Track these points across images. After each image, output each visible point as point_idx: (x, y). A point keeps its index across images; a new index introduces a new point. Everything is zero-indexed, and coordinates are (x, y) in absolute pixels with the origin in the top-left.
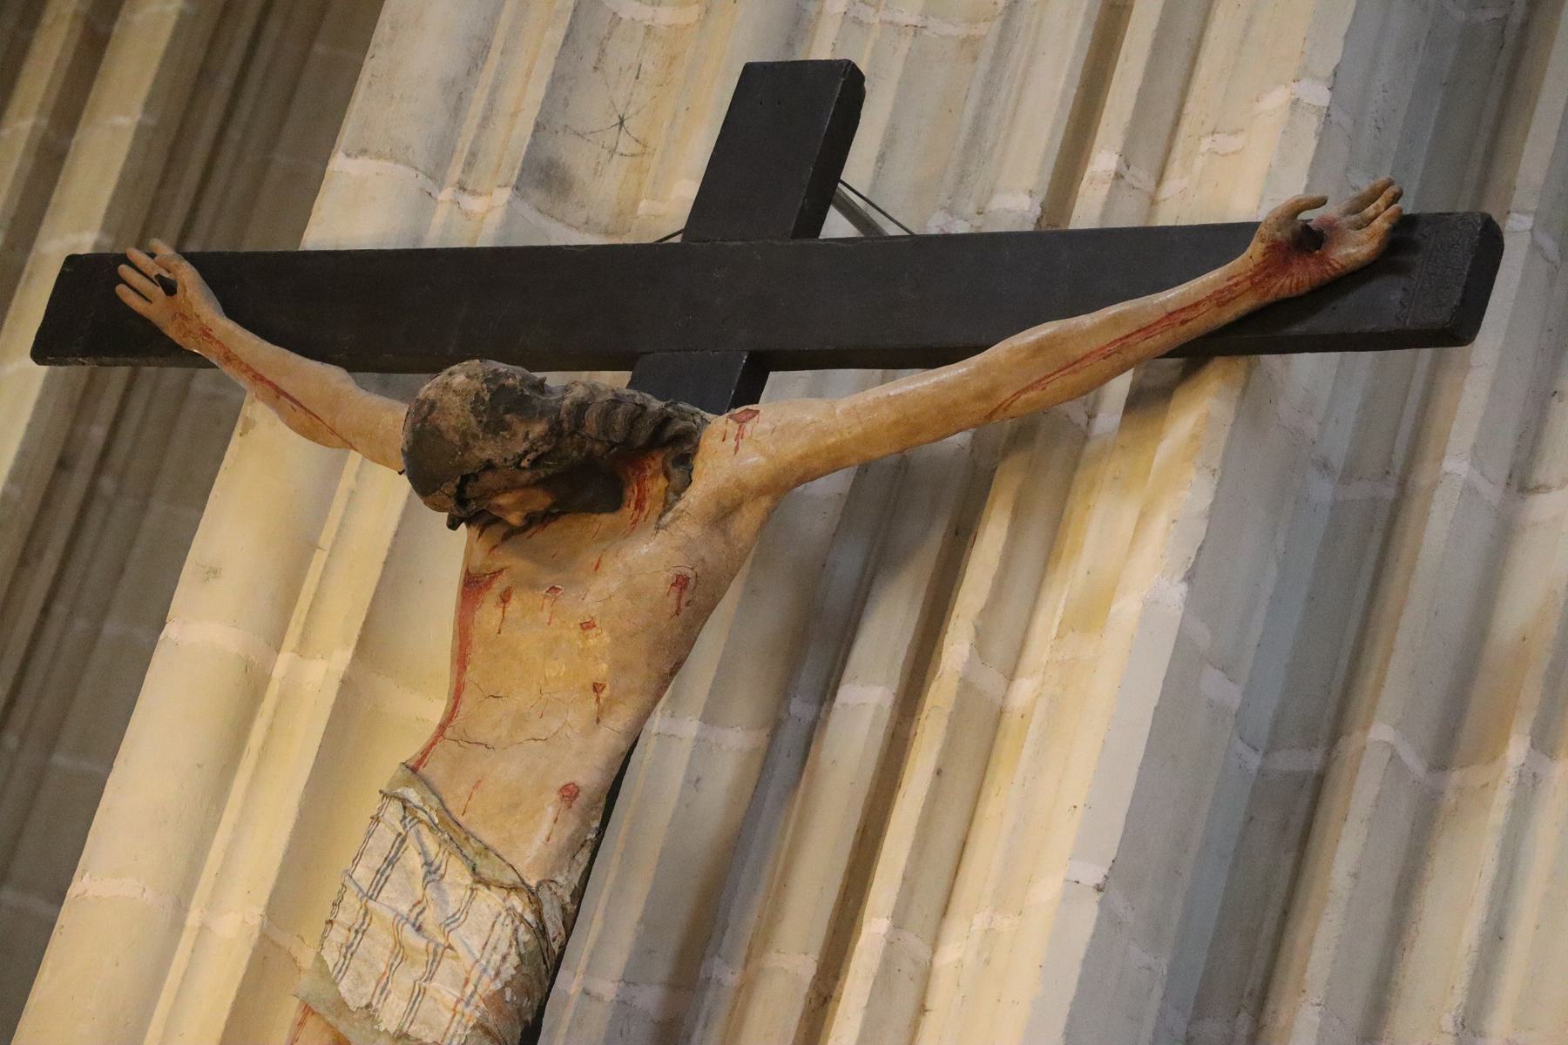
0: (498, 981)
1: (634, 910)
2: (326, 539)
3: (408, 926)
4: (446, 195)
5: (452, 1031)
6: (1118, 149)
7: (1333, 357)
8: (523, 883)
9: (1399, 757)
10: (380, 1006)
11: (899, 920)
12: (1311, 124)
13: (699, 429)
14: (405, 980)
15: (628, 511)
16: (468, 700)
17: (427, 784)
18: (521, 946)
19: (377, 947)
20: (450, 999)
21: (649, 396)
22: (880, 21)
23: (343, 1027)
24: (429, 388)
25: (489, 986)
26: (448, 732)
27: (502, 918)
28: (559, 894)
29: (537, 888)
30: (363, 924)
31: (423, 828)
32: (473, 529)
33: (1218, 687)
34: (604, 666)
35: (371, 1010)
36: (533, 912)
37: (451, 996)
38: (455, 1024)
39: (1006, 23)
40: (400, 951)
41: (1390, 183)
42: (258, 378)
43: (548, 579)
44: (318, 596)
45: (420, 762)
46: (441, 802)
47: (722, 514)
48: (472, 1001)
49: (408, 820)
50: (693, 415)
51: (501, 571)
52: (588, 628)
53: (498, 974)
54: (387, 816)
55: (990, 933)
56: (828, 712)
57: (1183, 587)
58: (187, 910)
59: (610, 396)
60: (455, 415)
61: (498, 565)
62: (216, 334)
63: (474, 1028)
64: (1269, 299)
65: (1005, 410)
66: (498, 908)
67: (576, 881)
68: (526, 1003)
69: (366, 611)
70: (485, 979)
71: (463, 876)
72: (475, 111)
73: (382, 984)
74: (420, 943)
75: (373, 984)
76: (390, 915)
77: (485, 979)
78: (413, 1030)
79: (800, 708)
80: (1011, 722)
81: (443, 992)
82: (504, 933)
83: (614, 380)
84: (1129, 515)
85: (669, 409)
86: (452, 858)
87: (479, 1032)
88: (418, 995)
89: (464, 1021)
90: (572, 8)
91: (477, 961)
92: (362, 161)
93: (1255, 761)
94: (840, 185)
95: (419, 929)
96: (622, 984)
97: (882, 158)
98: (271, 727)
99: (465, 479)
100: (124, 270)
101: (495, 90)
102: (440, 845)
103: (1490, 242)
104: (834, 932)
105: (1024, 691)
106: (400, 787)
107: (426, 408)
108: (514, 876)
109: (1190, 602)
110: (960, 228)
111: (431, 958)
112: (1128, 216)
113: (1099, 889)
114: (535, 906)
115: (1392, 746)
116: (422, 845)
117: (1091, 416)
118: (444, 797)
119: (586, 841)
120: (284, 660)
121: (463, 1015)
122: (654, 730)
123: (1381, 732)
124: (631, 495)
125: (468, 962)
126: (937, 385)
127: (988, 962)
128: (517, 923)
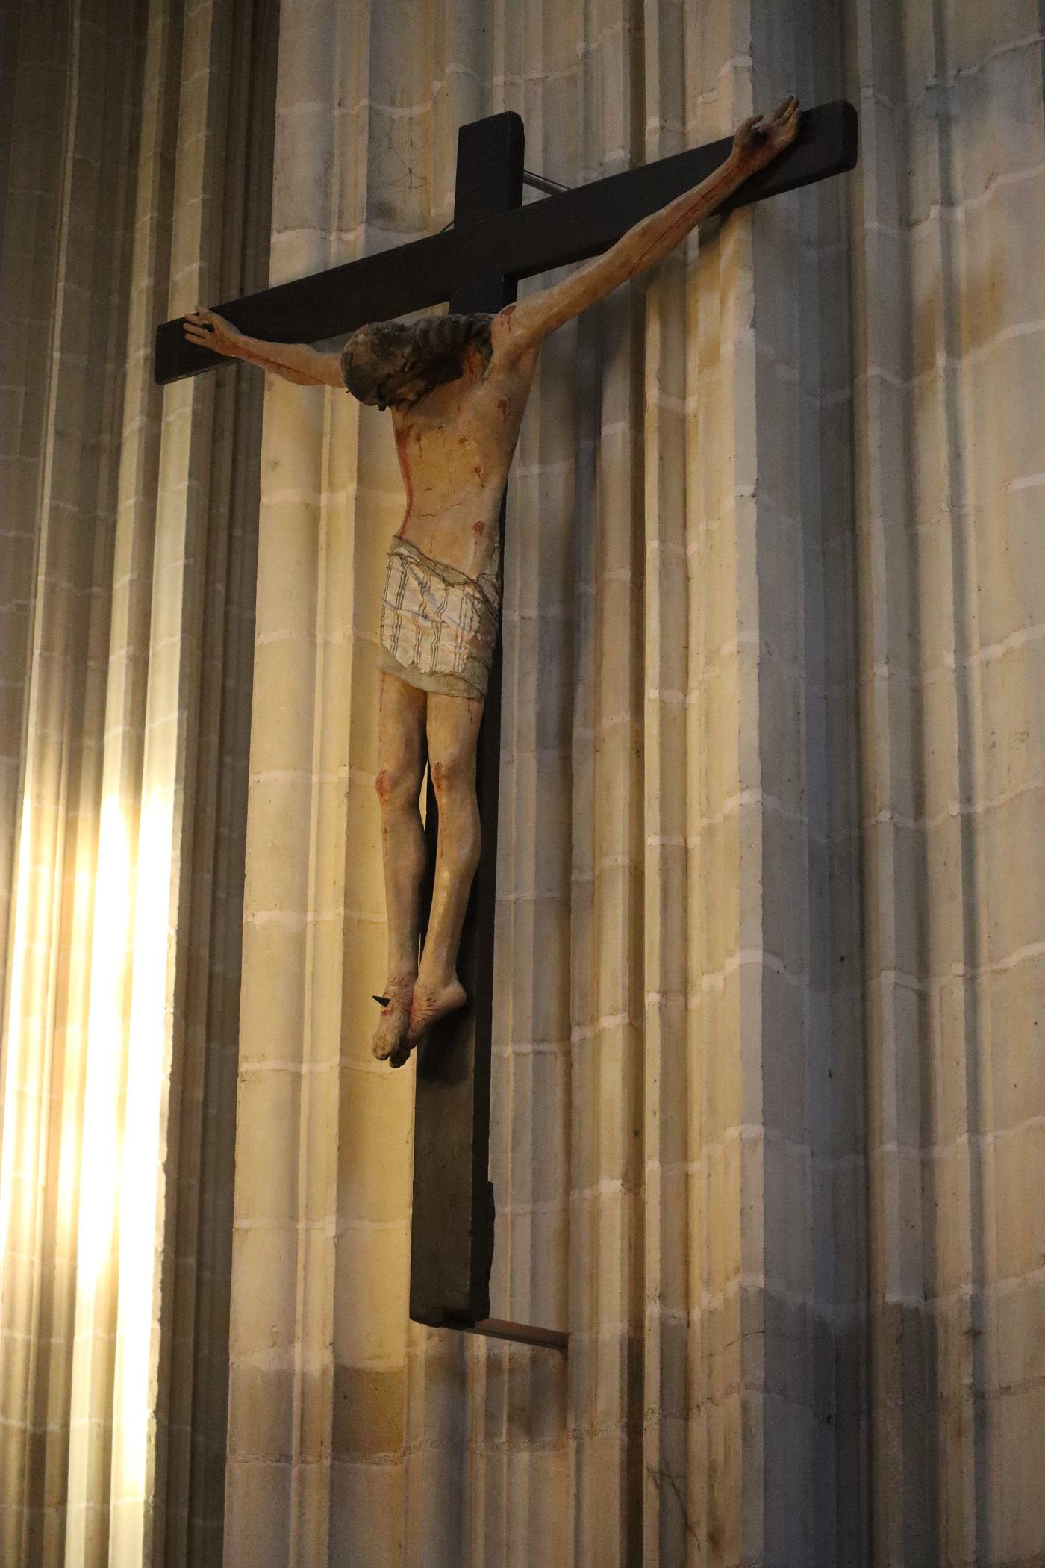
1: (534, 569)
2: (327, 428)
3: (420, 617)
4: (333, 236)
5: (457, 664)
7: (794, 193)
8: (470, 579)
9: (886, 380)
11: (663, 540)
12: (746, 77)
13: (489, 324)
14: (426, 645)
15: (467, 375)
16: (416, 494)
17: (409, 543)
18: (478, 611)
19: (409, 632)
20: (452, 648)
21: (458, 315)
23: (403, 677)
24: (348, 346)
25: (468, 636)
26: (411, 515)
27: (464, 600)
31: (413, 566)
34: (478, 458)
35: (415, 664)
36: (479, 592)
38: (457, 660)
39: (585, 64)
41: (792, 98)
42: (267, 361)
43: (437, 423)
44: (331, 460)
46: (418, 549)
47: (513, 363)
51: (412, 426)
52: (463, 441)
53: (470, 629)
54: (394, 565)
56: (600, 441)
57: (752, 331)
58: (315, 636)
60: (365, 358)
61: (409, 423)
62: (241, 345)
63: (467, 659)
64: (750, 173)
66: (461, 596)
67: (496, 570)
68: (489, 638)
70: (465, 633)
71: (440, 585)
72: (335, 189)
73: (416, 650)
74: (428, 624)
75: (412, 650)
76: (410, 615)
78: (438, 668)
79: (586, 444)
80: (690, 420)
82: (467, 607)
83: (439, 310)
85: (471, 319)
86: (432, 577)
87: (471, 659)
88: (435, 651)
90: (368, 122)
91: (459, 625)
93: (818, 403)
95: (426, 617)
99: (380, 386)
100: (186, 326)
101: (342, 175)
103: (849, 116)
105: (692, 403)
106: (395, 548)
107: (349, 357)
113: (754, 496)
116: (415, 574)
117: (685, 253)
122: (518, 476)
123: (873, 371)
124: (466, 366)
125: (454, 627)
126: (600, 266)
127: (711, 547)
128: (472, 600)
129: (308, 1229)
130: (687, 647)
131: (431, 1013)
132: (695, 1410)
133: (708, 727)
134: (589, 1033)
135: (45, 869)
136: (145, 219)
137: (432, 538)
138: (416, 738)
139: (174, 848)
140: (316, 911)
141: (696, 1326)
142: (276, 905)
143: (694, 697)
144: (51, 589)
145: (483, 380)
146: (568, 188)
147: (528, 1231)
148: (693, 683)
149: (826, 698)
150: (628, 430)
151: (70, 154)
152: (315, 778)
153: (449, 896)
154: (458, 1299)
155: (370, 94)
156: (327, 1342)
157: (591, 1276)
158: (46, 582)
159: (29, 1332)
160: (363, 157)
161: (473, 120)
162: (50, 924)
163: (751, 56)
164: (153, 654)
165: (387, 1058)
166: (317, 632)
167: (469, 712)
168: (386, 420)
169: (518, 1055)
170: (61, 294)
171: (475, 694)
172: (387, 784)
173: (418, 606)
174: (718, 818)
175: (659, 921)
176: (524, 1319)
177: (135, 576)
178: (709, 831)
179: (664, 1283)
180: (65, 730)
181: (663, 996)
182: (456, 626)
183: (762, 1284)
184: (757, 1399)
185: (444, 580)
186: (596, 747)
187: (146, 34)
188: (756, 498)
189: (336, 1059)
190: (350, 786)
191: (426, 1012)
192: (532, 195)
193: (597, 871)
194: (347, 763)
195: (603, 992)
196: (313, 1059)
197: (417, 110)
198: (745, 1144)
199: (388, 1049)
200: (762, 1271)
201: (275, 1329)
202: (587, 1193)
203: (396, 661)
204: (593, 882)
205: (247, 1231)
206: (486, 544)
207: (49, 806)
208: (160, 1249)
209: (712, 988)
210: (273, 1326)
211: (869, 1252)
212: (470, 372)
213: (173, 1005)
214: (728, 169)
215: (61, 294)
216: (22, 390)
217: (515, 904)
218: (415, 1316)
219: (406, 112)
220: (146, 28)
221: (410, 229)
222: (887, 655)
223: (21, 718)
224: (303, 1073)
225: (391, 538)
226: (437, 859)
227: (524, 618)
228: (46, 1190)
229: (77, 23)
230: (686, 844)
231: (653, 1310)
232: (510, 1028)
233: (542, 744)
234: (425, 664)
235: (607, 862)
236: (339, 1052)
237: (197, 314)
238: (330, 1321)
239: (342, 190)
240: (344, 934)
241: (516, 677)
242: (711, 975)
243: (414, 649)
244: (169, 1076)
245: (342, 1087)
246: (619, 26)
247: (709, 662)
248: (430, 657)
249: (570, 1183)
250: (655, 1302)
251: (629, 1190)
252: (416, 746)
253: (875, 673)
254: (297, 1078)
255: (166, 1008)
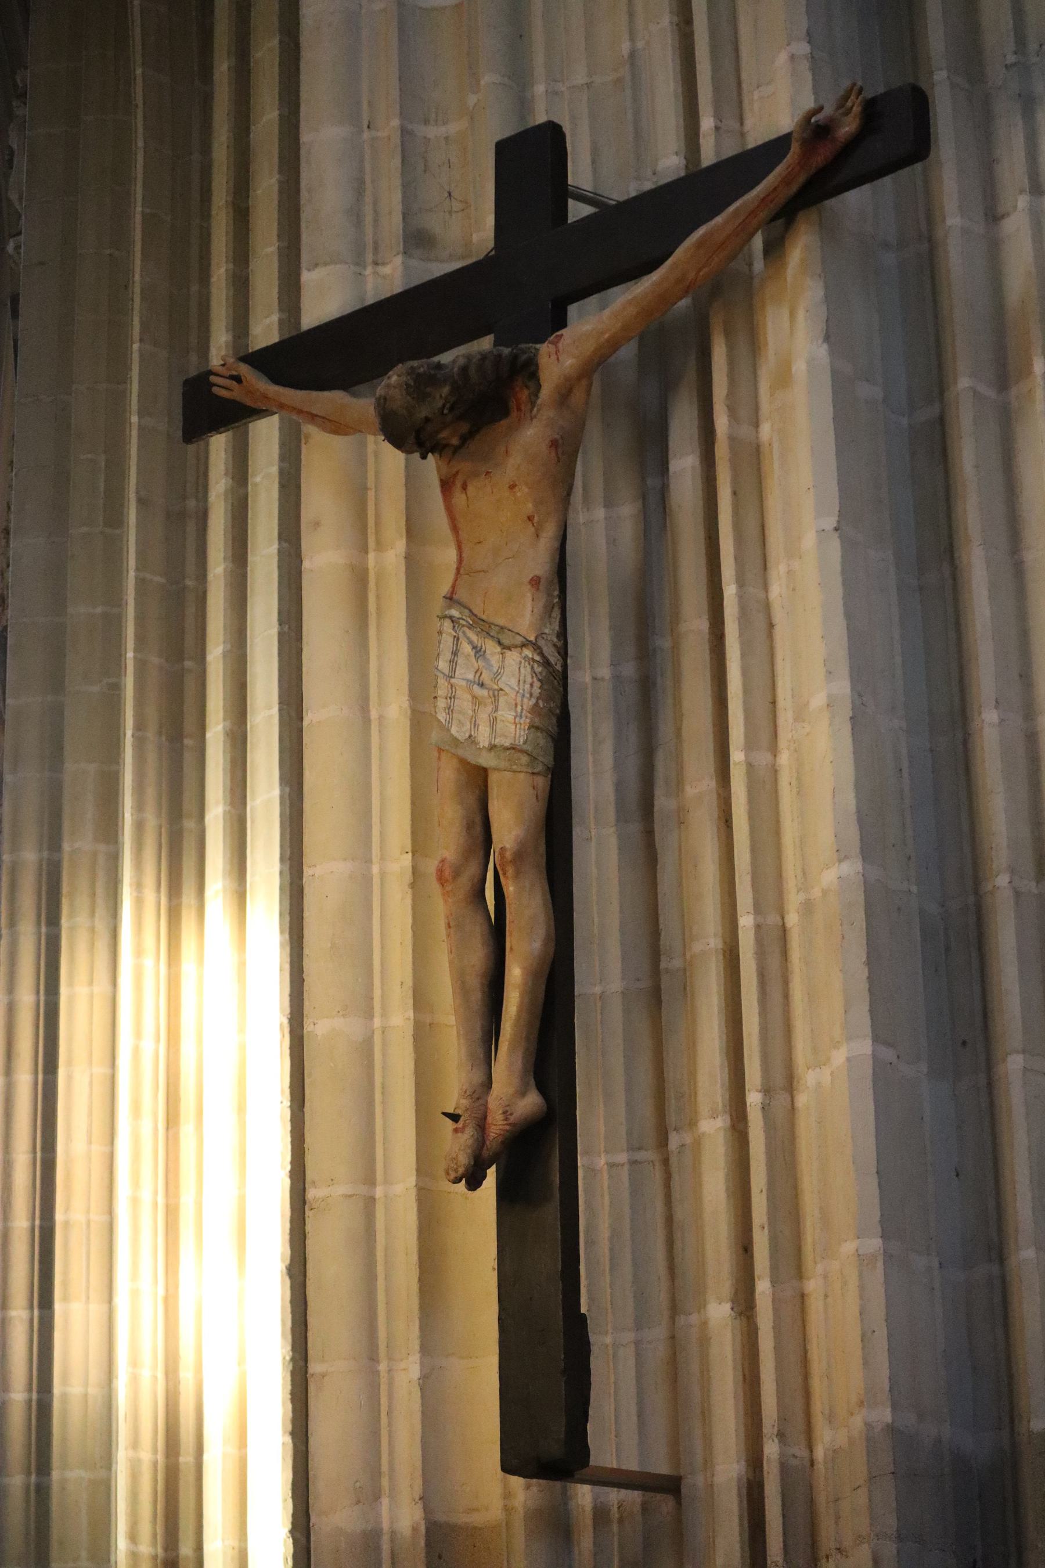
0: (532, 699)
2: (371, 482)
3: (475, 686)
4: (369, 271)
5: (518, 733)
6: (712, 113)
7: (866, 188)
8: (527, 640)
10: (476, 734)
11: (741, 582)
12: (804, 67)
14: (483, 716)
15: (514, 414)
17: (460, 604)
18: (539, 675)
19: (464, 702)
20: (511, 718)
22: (567, 88)
23: (460, 752)
24: (380, 390)
26: (462, 571)
27: (523, 664)
28: (549, 639)
29: (536, 640)
30: (452, 693)
31: (466, 629)
32: (436, 455)
33: (867, 391)
34: (530, 505)
36: (538, 654)
37: (510, 716)
38: (518, 731)
39: (632, 64)
40: (475, 699)
41: (854, 84)
45: (452, 593)
47: (564, 396)
48: (523, 714)
49: (456, 627)
50: (529, 349)
51: (457, 472)
53: (531, 695)
55: (790, 572)
57: (825, 346)
58: (368, 711)
59: (479, 357)
60: (399, 399)
61: (454, 470)
62: (270, 395)
65: (694, 284)
67: (557, 628)
69: (405, 515)
70: (525, 700)
72: (369, 219)
73: (473, 722)
74: (484, 693)
75: (468, 723)
76: (464, 683)
77: (525, 700)
78: (497, 741)
81: (506, 715)
82: (526, 671)
83: (486, 343)
84: (785, 313)
85: (515, 351)
86: (486, 640)
87: (533, 730)
88: (493, 722)
89: (522, 727)
91: (518, 692)
92: (317, 270)
93: (905, 421)
94: (569, 187)
95: (482, 685)
96: (612, 667)
97: (593, 162)
98: (378, 597)
100: (213, 379)
101: (375, 203)
102: (477, 635)
104: (713, 598)
105: (766, 430)
108: (521, 639)
109: (832, 352)
110: (648, 186)
111: (493, 699)
112: (730, 150)
113: (836, 529)
114: (538, 651)
115: (971, 388)
116: (468, 638)
117: (750, 265)
118: (471, 608)
119: (554, 605)
120: (371, 556)
121: (521, 724)
123: (964, 383)
124: (513, 404)
125: (513, 695)
127: (794, 590)
128: (532, 663)
129: (390, 1371)
130: (774, 703)
131: (507, 1128)
132: (824, 1561)
133: (800, 792)
134: (688, 1138)
135: (148, 962)
136: (220, 273)
137: (485, 596)
138: (478, 819)
139: (282, 932)
140: (384, 1015)
141: (820, 1467)
142: (339, 1012)
143: (784, 759)
144: (141, 665)
145: (532, 419)
146: (617, 201)
147: (631, 1362)
148: (783, 742)
149: (932, 751)
150: (697, 463)
151: (139, 209)
152: (375, 869)
153: (522, 996)
154: (554, 1447)
155: (401, 114)
156: (417, 1498)
157: (703, 1413)
158: (135, 658)
159: (155, 1451)
160: (397, 182)
161: (507, 133)
162: (157, 1018)
163: (809, 42)
164: (251, 728)
165: (460, 1181)
166: (371, 708)
167: (534, 788)
168: (431, 466)
169: (612, 1166)
170: (136, 356)
171: (539, 768)
172: (447, 873)
173: (473, 673)
174: (816, 893)
175: (757, 1011)
176: (632, 1464)
177: (229, 646)
178: (808, 908)
179: (783, 1419)
180: (164, 810)
181: (765, 1095)
182: (515, 694)
183: (888, 1419)
184: (890, 1549)
185: (500, 643)
186: (681, 818)
187: (212, 81)
188: (839, 531)
189: (412, 1180)
190: (414, 873)
191: (501, 1127)
192: (577, 211)
193: (688, 957)
194: (409, 850)
195: (701, 1092)
196: (387, 1182)
197: (454, 128)
198: (862, 1260)
199: (461, 1170)
200: (889, 1403)
201: (358, 1485)
202: (694, 1319)
203: (452, 735)
204: (685, 969)
205: (323, 1376)
206: (544, 600)
207: (150, 895)
208: (288, 1358)
209: (819, 1085)
210: (357, 1482)
211: (1011, 1377)
212: (518, 411)
213: (289, 1098)
214: (787, 168)
215: (136, 356)
216: (102, 459)
217: (600, 997)
218: (507, 1468)
219: (442, 130)
220: (212, 75)
221: (451, 258)
222: (997, 699)
223: (117, 803)
224: (377, 1197)
225: (442, 600)
226: (507, 953)
227: (596, 679)
228: (166, 1299)
229: (139, 71)
230: (784, 923)
231: (771, 1449)
232: (602, 1136)
233: (622, 816)
234: (484, 737)
235: (697, 947)
236: (415, 1173)
237: (223, 365)
238: (419, 1473)
239: (376, 221)
240: (415, 1040)
241: (590, 747)
242: (818, 1070)
243: (471, 722)
244: (288, 1174)
245: (420, 1211)
246: (665, 21)
247: (798, 718)
248: (488, 729)
249: (674, 1309)
250: (773, 1441)
251: (741, 1314)
252: (478, 829)
253: (983, 721)
254: (370, 1202)
255: (282, 1102)
